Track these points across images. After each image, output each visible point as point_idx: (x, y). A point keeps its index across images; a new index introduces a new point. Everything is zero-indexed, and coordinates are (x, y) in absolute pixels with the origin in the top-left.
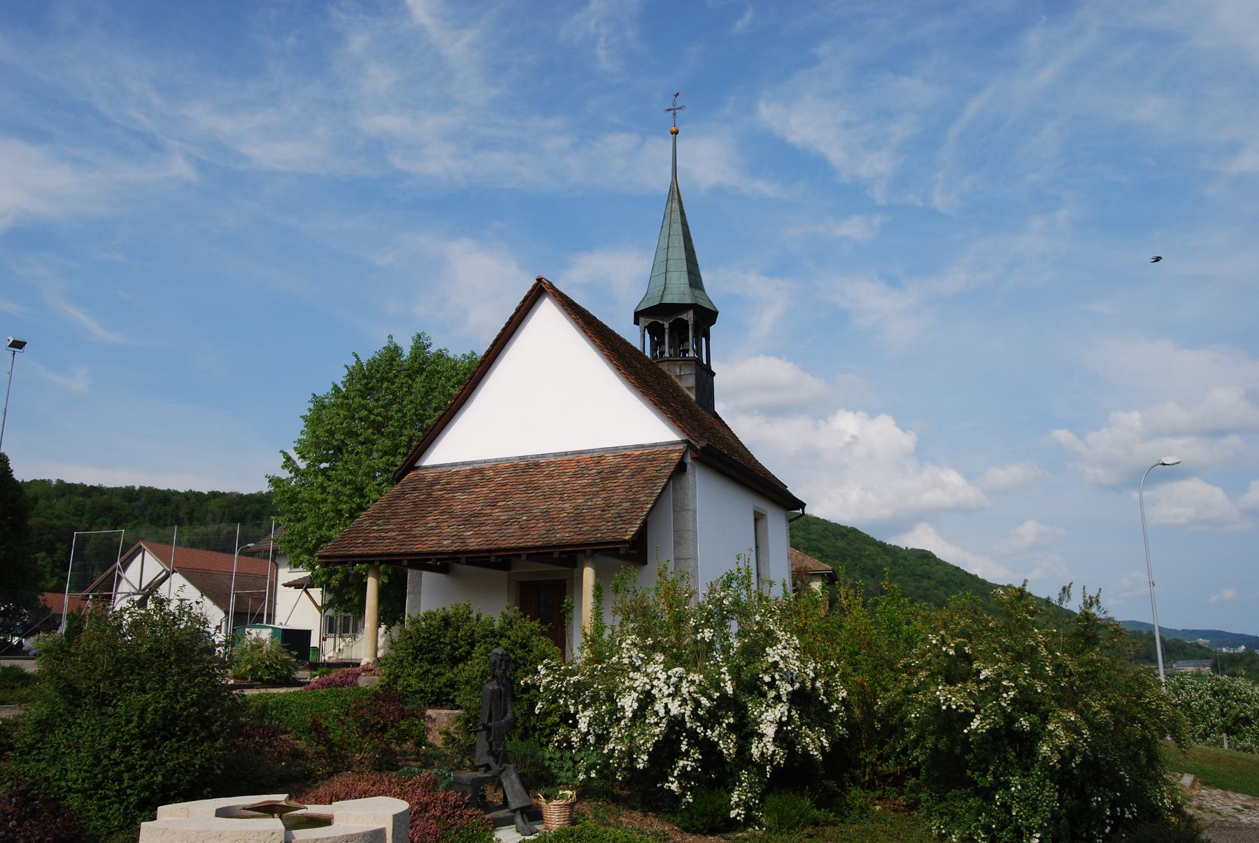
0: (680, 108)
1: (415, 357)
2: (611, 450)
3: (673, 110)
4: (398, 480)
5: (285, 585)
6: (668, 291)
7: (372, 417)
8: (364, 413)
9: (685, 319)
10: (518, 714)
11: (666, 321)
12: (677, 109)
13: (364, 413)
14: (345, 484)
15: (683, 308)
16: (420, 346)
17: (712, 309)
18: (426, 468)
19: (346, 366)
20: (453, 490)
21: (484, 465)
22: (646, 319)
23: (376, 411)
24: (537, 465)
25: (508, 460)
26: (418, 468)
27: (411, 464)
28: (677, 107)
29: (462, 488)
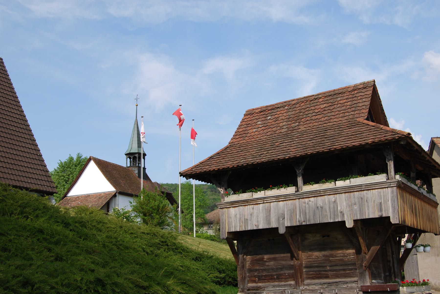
0: (136, 99)
1: (77, 161)
4: (63, 199)
5: (336, 185)
7: (65, 179)
8: (62, 177)
10: (111, 244)
13: (62, 177)
14: (58, 198)
15: (135, 153)
16: (79, 157)
18: (69, 196)
19: (58, 163)
20: (72, 201)
21: (80, 196)
23: (66, 177)
24: (89, 196)
25: (84, 195)
26: (67, 196)
27: (65, 196)
29: (74, 201)
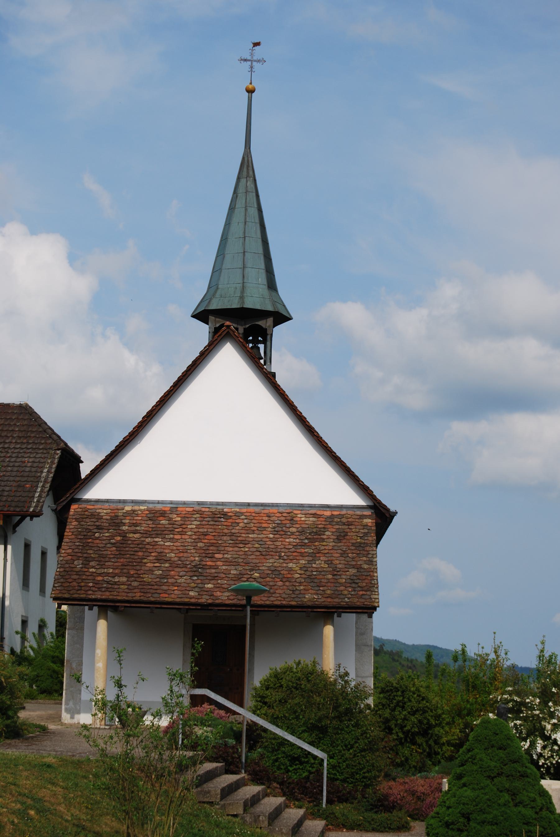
2: (295, 507)
3: (250, 61)
6: (248, 292)
9: (264, 326)
11: (242, 325)
12: (255, 61)
17: (289, 316)
18: (88, 501)
22: (217, 319)
26: (79, 500)
28: (255, 58)
